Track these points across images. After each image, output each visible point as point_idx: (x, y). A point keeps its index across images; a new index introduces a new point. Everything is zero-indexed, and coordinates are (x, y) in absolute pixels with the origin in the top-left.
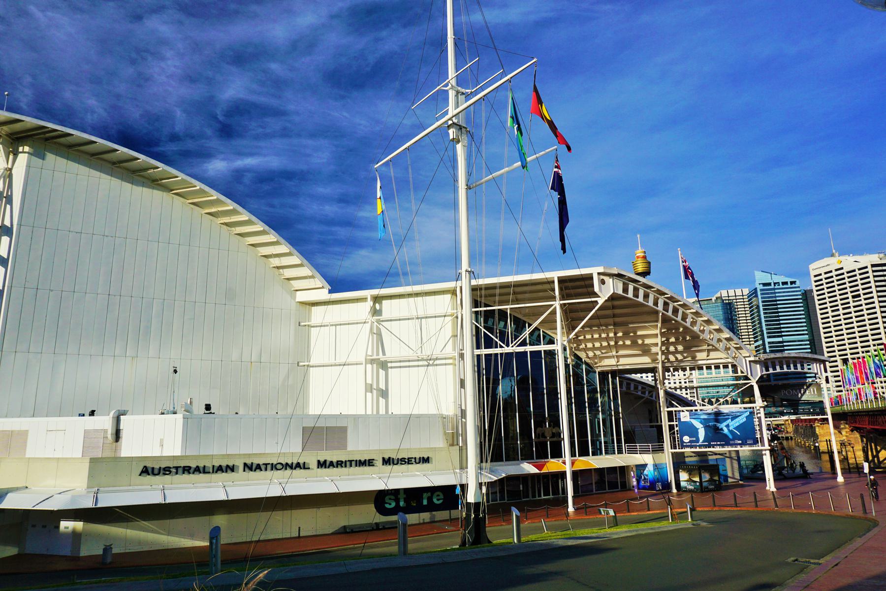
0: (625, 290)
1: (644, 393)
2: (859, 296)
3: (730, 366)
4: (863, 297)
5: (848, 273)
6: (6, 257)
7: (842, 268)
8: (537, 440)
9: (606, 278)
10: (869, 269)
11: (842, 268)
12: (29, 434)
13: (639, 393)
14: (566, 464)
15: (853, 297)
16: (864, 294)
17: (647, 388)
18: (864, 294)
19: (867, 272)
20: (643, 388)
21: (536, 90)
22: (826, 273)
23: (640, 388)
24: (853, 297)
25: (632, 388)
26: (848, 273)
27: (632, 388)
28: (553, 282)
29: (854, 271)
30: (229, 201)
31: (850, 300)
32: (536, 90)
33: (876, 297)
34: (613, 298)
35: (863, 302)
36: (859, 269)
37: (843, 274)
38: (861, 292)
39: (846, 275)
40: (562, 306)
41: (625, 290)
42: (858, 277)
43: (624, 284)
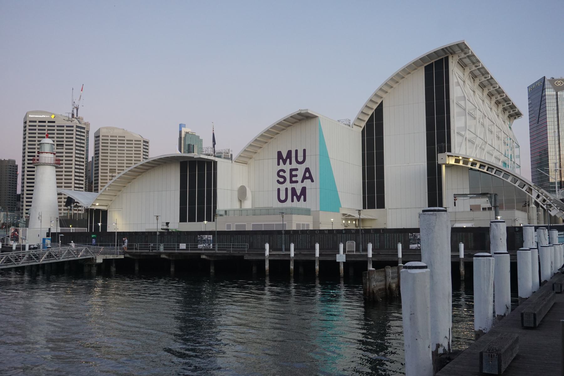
5: (58, 126)
7: (54, 122)
11: (54, 122)
12: (309, 216)
15: (57, 145)
16: (66, 145)
18: (66, 145)
19: (72, 149)
21: (213, 134)
24: (57, 145)
26: (58, 126)
29: (63, 126)
30: (81, 258)
32: (213, 134)
33: (73, 175)
35: (64, 150)
36: (67, 126)
37: (54, 126)
38: (65, 143)
39: (56, 128)
42: (65, 132)
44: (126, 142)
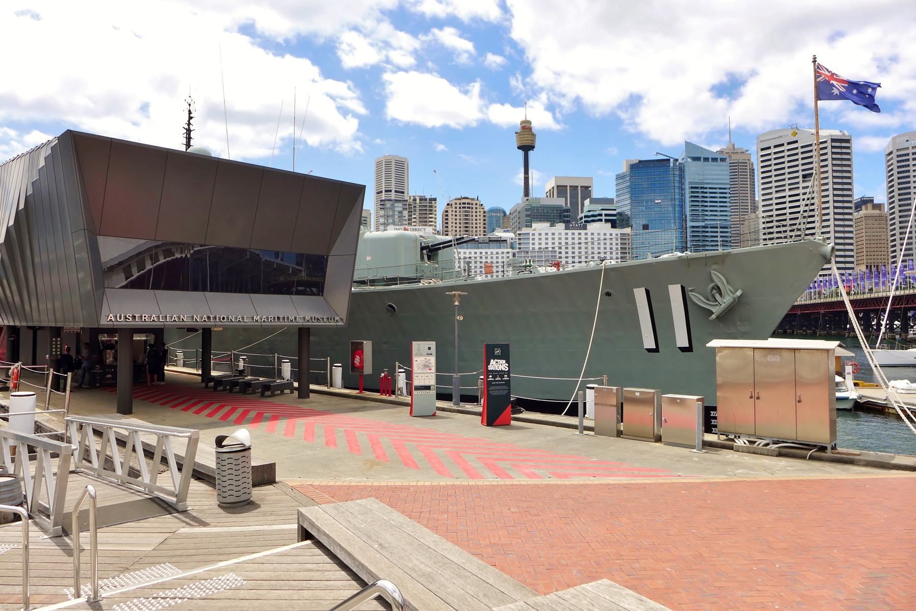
5: (802, 147)
7: (796, 142)
10: (829, 145)
11: (796, 142)
24: (804, 176)
31: (801, 179)
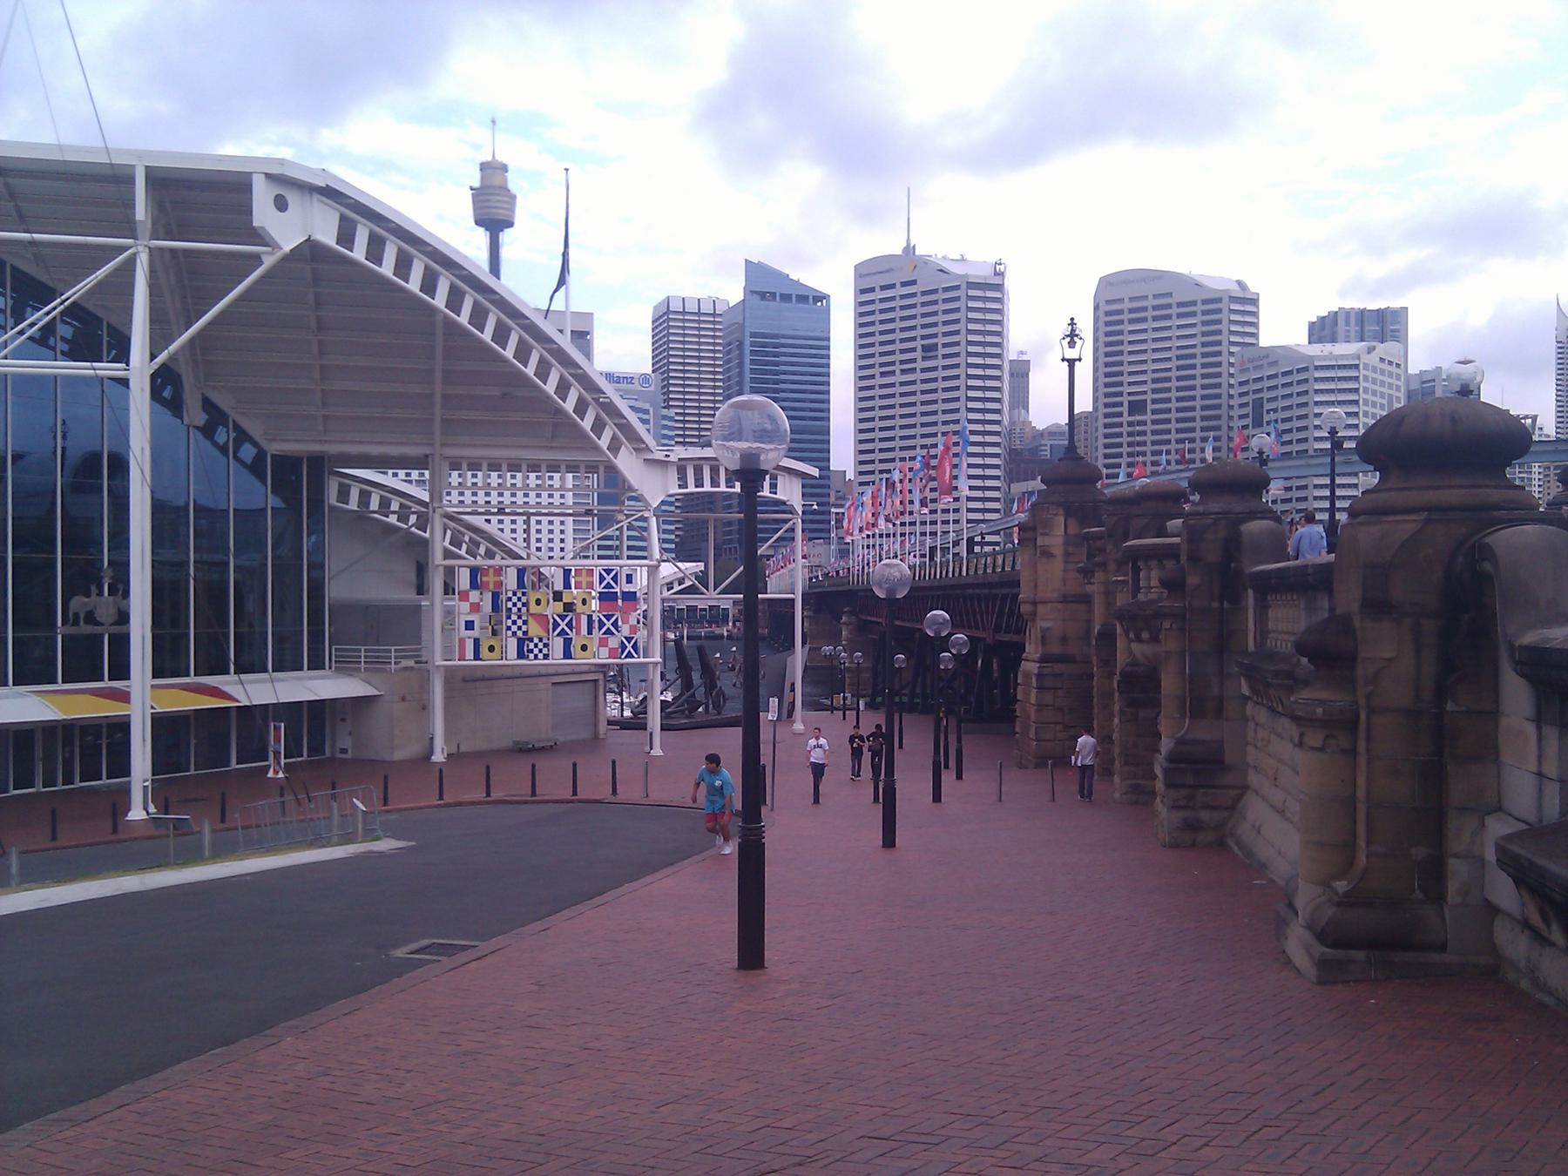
0: (346, 237)
1: (403, 518)
2: (934, 347)
3: (602, 469)
4: (942, 351)
5: (924, 293)
6: (1525, 827)
7: (914, 282)
8: (70, 630)
9: (293, 198)
11: (914, 282)
13: (393, 519)
14: (144, 697)
15: (924, 348)
16: (945, 345)
17: (415, 508)
18: (945, 345)
20: (362, 492)
22: (883, 288)
23: (395, 506)
24: (924, 348)
25: (374, 504)
27: (374, 504)
28: (131, 181)
31: (918, 354)
34: (311, 251)
37: (1169, 306)
40: (152, 251)
41: (346, 237)
43: (343, 218)
44: (1175, 311)
